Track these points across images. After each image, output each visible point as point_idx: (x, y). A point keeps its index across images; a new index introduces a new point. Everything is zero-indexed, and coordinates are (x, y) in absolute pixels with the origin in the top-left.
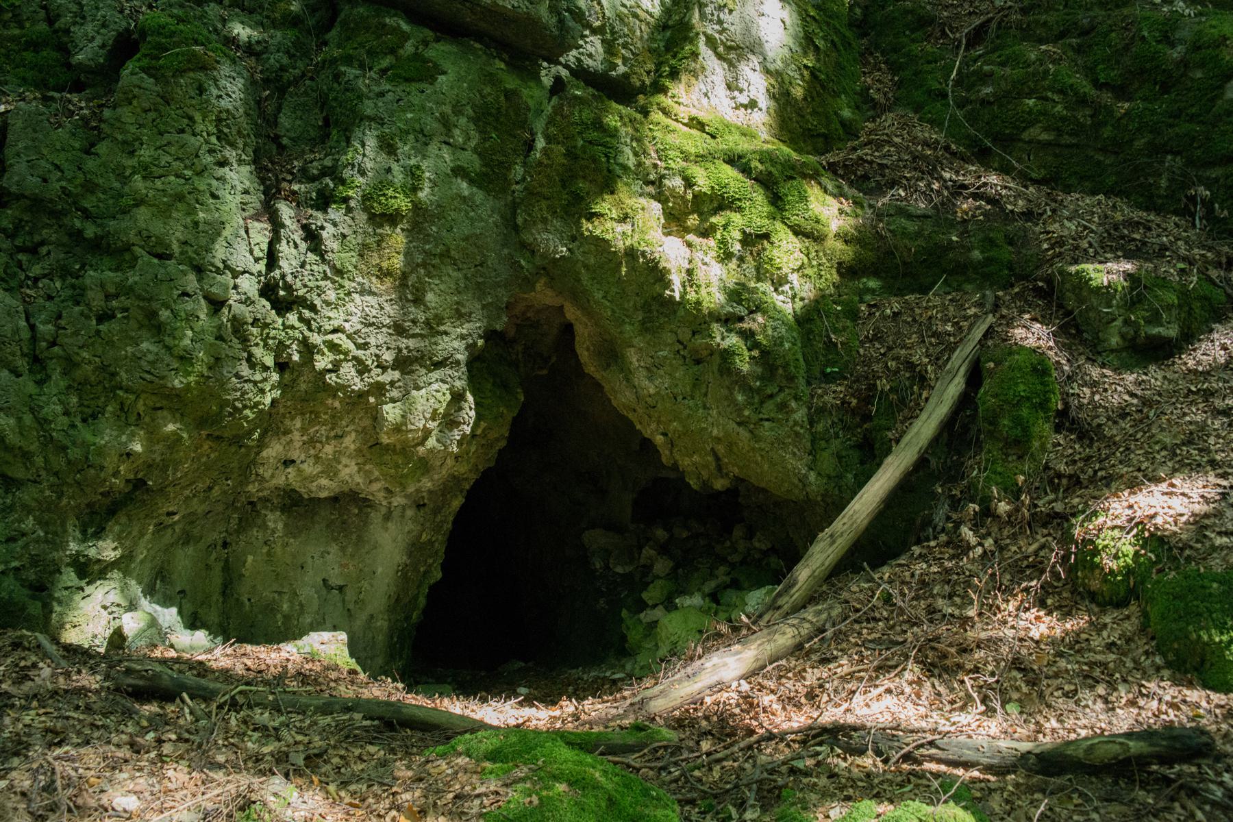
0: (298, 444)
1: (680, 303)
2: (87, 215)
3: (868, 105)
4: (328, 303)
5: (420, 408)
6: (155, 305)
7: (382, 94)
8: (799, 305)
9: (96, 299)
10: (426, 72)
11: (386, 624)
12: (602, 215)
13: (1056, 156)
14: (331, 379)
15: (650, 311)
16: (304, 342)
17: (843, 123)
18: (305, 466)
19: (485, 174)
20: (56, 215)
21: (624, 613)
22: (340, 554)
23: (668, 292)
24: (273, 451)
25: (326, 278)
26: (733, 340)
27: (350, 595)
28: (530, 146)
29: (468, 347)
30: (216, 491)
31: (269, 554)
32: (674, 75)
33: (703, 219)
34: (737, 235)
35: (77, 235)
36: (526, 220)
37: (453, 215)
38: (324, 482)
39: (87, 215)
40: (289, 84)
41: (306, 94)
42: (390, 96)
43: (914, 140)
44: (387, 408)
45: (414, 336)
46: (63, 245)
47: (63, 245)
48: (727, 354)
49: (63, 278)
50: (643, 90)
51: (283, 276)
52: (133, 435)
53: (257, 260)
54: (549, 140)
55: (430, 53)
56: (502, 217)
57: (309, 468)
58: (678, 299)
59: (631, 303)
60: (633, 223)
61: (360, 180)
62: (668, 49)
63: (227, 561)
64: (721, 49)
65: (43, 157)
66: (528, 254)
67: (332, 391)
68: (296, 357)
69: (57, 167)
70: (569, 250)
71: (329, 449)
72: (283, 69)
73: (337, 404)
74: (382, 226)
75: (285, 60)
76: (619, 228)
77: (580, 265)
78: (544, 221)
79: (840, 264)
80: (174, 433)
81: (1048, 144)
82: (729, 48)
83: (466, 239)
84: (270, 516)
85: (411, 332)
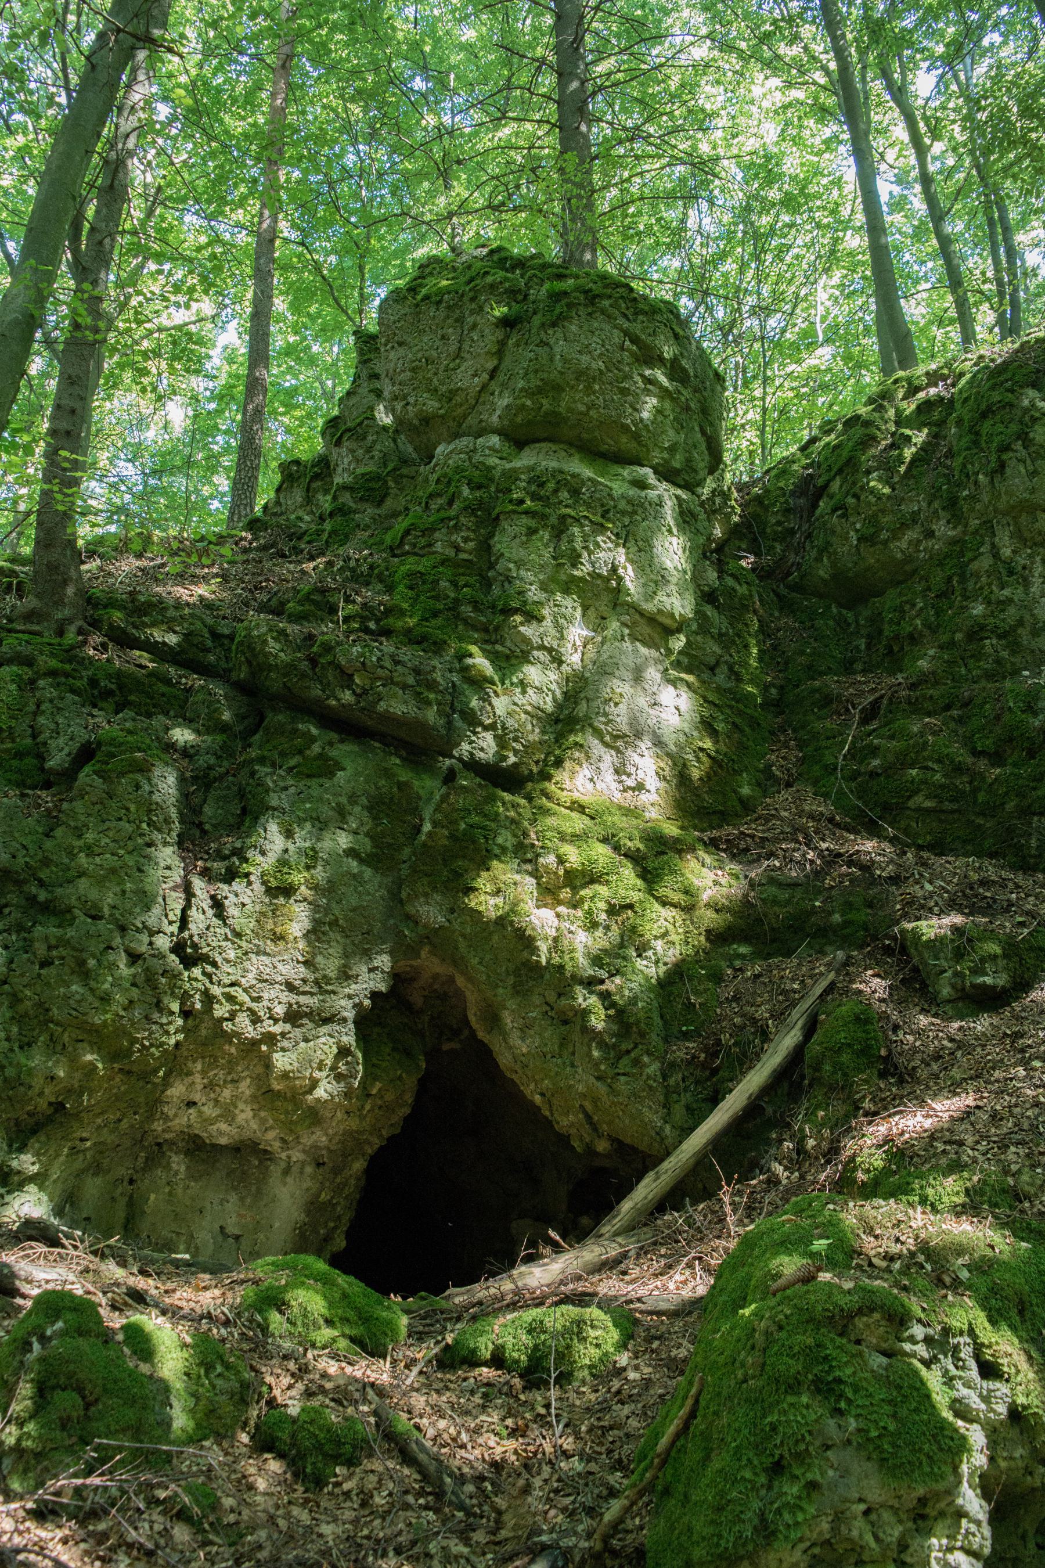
0: (199, 1087)
2: (41, 883)
3: (767, 782)
4: (228, 961)
6: (84, 955)
7: (286, 788)
8: (662, 969)
9: (41, 949)
10: (326, 768)
13: (941, 821)
14: (227, 1026)
16: (206, 993)
17: (741, 801)
18: (205, 1109)
19: (376, 855)
20: (19, 883)
24: (177, 1091)
25: (226, 939)
26: (593, 1000)
28: (418, 829)
29: (355, 1006)
30: (124, 1124)
31: (170, 1194)
32: (559, 763)
33: (575, 889)
34: (602, 905)
35: (32, 899)
37: (343, 889)
38: (223, 1126)
39: (41, 883)
40: (215, 780)
41: (228, 788)
42: (292, 790)
43: (801, 813)
44: (276, 1056)
45: (304, 993)
48: (585, 1013)
49: (18, 932)
50: (531, 777)
51: (191, 936)
52: (58, 1061)
53: (171, 923)
54: (435, 824)
55: (334, 753)
57: (209, 1111)
60: (503, 890)
61: (259, 859)
62: (557, 741)
63: (131, 1197)
64: (608, 738)
65: (15, 839)
67: (228, 1037)
68: (198, 1006)
69: (24, 847)
71: (227, 1093)
72: (210, 768)
73: (233, 1050)
74: (276, 897)
75: (212, 761)
76: (492, 901)
78: (426, 895)
79: (708, 932)
80: (91, 1063)
81: (928, 811)
82: (617, 737)
83: (354, 910)
84: (175, 1158)
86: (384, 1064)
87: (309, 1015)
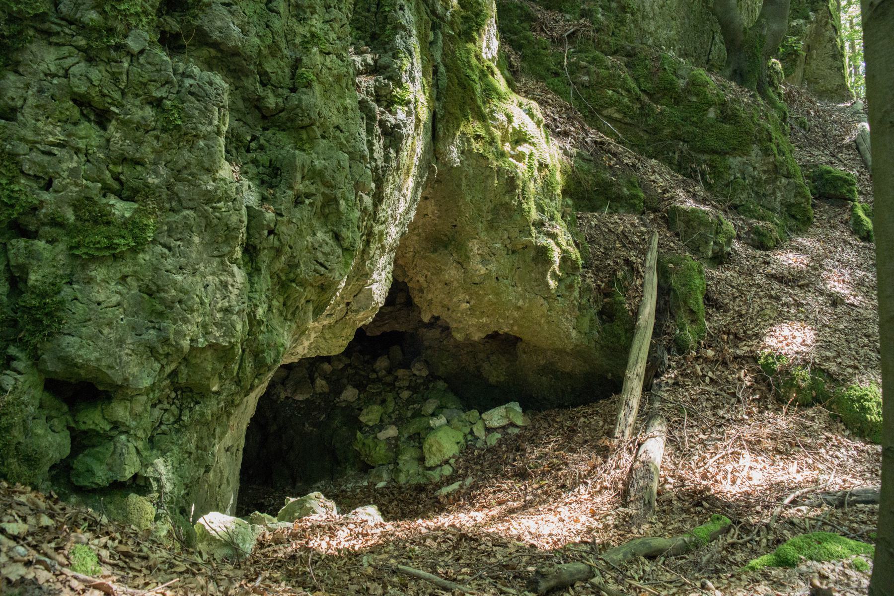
15: (498, 214)
46: (238, 111)
47: (238, 111)
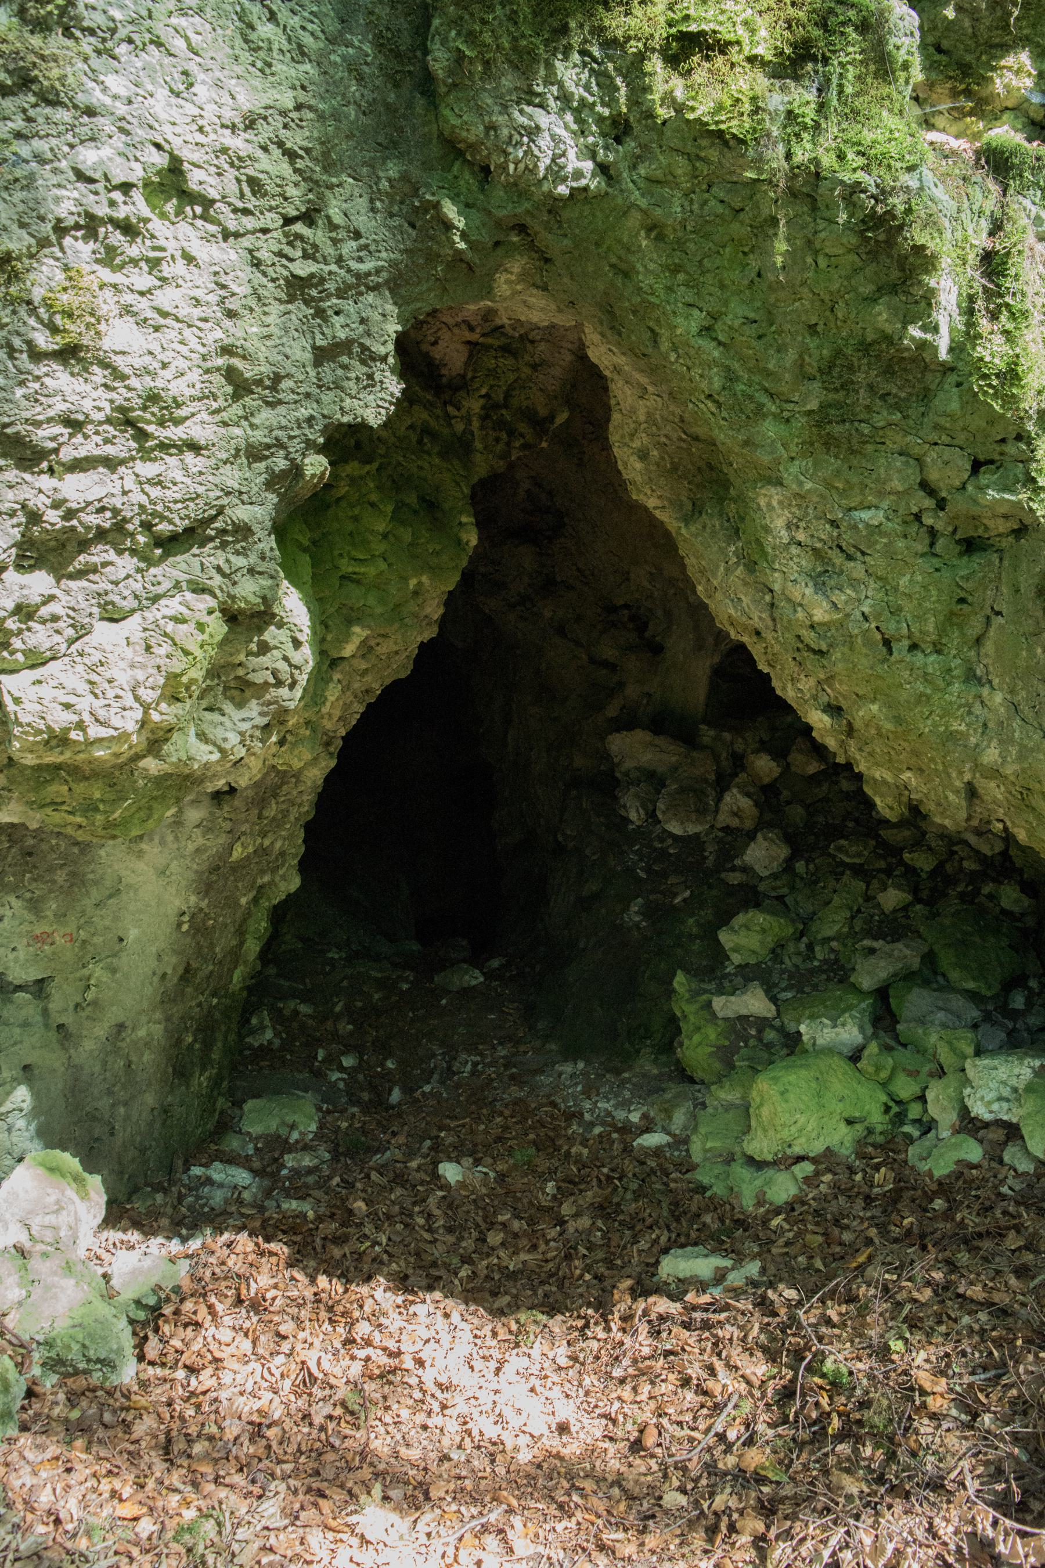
1: (947, 369)
5: (123, 678)
11: (158, 1030)
12: (724, 47)
21: (680, 981)
22: (29, 916)
23: (915, 331)
27: (59, 1001)
36: (460, 58)
45: (78, 466)
56: (380, 45)
58: (943, 355)
59: (792, 355)
66: (468, 179)
70: (603, 169)
77: (634, 220)
85: (67, 454)
86: (370, 571)
87: (116, 533)
